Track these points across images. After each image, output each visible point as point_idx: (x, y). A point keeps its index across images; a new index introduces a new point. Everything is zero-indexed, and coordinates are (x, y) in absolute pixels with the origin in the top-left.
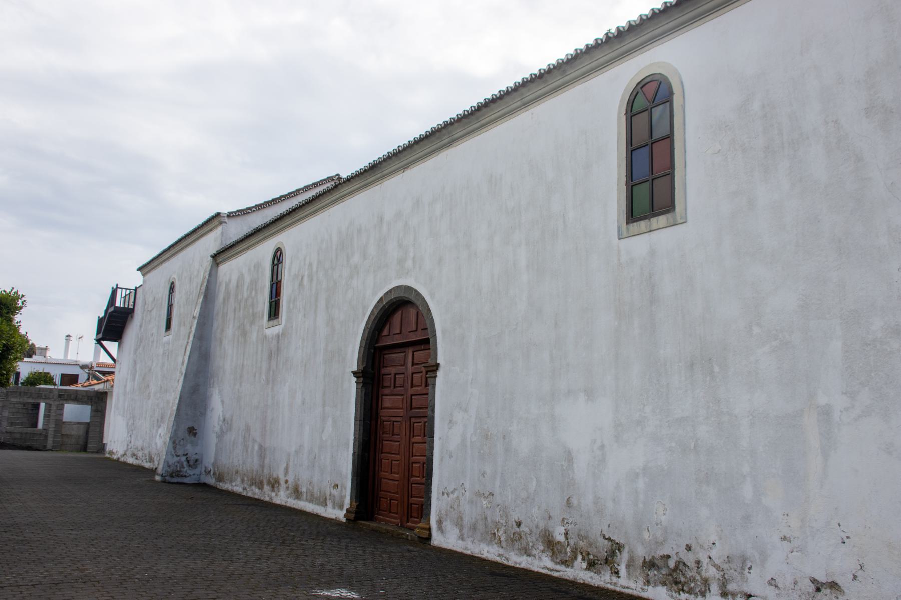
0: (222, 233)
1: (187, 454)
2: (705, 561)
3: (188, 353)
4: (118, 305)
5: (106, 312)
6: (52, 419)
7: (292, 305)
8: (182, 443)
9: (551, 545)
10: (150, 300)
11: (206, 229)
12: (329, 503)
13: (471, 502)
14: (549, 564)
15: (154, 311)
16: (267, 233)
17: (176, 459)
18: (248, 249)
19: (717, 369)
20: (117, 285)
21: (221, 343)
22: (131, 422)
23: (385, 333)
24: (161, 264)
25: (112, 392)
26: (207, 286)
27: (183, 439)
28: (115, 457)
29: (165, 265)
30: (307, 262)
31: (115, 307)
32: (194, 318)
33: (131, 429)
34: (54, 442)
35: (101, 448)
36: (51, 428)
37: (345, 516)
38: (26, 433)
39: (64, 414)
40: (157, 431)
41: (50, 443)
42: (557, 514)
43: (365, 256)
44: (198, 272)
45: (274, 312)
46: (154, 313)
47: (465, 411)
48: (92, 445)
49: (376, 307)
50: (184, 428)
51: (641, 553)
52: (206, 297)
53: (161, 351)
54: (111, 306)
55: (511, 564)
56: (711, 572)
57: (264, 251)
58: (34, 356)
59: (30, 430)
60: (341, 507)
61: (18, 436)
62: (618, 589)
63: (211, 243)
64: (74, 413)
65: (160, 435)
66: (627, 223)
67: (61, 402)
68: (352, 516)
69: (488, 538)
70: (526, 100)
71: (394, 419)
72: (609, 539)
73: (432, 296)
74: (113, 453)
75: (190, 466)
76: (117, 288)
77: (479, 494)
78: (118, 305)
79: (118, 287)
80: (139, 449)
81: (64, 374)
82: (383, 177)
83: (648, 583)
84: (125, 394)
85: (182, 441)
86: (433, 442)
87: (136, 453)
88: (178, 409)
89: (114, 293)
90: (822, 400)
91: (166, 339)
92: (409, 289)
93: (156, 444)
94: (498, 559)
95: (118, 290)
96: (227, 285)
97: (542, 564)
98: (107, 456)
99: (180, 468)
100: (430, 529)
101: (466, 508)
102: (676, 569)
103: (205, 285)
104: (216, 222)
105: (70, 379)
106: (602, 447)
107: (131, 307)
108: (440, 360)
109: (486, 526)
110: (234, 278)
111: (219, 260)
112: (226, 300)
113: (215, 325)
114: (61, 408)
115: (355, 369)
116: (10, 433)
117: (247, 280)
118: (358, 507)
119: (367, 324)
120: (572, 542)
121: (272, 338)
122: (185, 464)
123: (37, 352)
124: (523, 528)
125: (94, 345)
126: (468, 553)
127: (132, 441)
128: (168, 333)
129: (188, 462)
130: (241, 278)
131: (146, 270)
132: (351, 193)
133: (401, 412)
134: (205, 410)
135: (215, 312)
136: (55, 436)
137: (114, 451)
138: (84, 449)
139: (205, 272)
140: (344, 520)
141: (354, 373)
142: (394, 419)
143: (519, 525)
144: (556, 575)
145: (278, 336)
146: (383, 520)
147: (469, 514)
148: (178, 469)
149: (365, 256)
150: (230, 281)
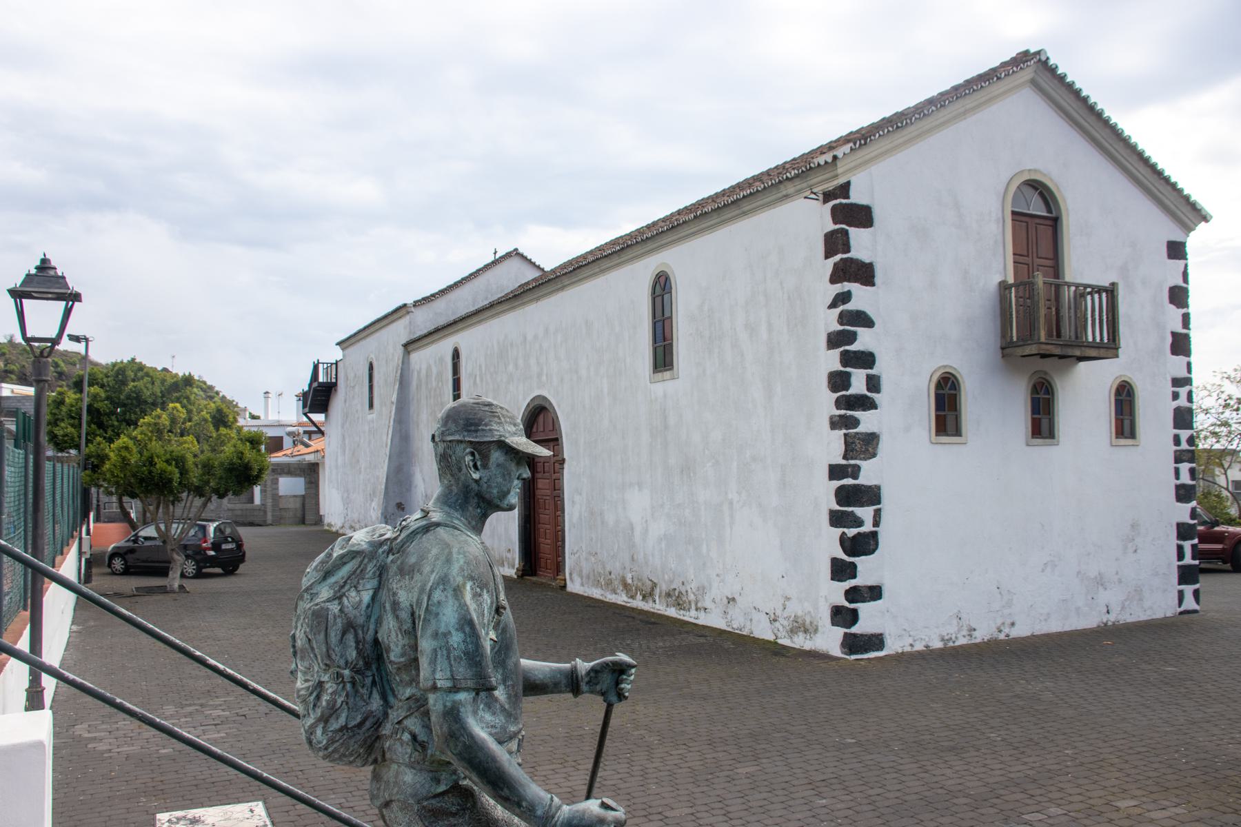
0: (410, 322)
2: (689, 590)
3: (390, 436)
4: (321, 379)
5: (310, 385)
6: (269, 494)
8: (392, 517)
9: (626, 586)
10: (351, 376)
11: (395, 316)
12: (505, 564)
13: (587, 559)
14: (625, 598)
15: (357, 387)
16: (446, 332)
18: (433, 342)
19: (692, 475)
21: (418, 426)
22: (346, 495)
23: (534, 430)
24: (358, 341)
25: (324, 463)
26: (401, 374)
28: (334, 529)
29: (363, 343)
31: (319, 383)
32: (392, 403)
33: (347, 502)
34: (273, 515)
35: (319, 520)
36: (269, 502)
37: (516, 574)
38: (247, 510)
39: (280, 488)
40: (370, 505)
41: (269, 518)
42: (628, 565)
43: (516, 366)
44: (393, 355)
46: (357, 389)
47: (580, 494)
48: (310, 517)
49: (525, 410)
50: (393, 504)
51: (664, 588)
52: (401, 383)
53: (367, 428)
54: (315, 381)
55: (607, 600)
56: (692, 597)
57: (444, 347)
59: (249, 506)
60: (513, 567)
61: (239, 513)
62: (656, 611)
63: (399, 332)
64: (289, 486)
67: (276, 476)
68: (520, 573)
69: (596, 583)
70: (602, 268)
71: (545, 498)
72: (651, 580)
73: (559, 406)
74: (332, 525)
76: (319, 363)
77: (590, 554)
78: (321, 379)
80: (356, 521)
82: (524, 304)
83: (667, 606)
84: (337, 467)
86: (564, 516)
87: (353, 525)
88: (386, 488)
89: (316, 368)
90: (730, 496)
91: (370, 417)
92: (544, 398)
93: (371, 517)
94: (601, 598)
96: (419, 373)
97: (621, 599)
98: (326, 528)
100: (565, 580)
101: (584, 564)
102: (678, 597)
103: (399, 372)
104: (403, 311)
107: (334, 380)
108: (566, 456)
109: (594, 575)
110: (424, 367)
111: (410, 348)
112: (419, 387)
113: (412, 409)
114: (276, 482)
116: (232, 510)
117: (434, 371)
118: (524, 566)
120: (635, 583)
124: (613, 576)
126: (586, 595)
127: (349, 513)
128: (371, 411)
130: (429, 368)
131: (345, 345)
132: (504, 312)
133: (548, 492)
134: (410, 486)
135: (411, 398)
136: (273, 511)
137: (333, 523)
138: (303, 521)
139: (398, 359)
140: (516, 577)
142: (545, 498)
143: (610, 573)
144: (628, 605)
146: (542, 575)
147: (586, 567)
149: (516, 366)
150: (420, 369)
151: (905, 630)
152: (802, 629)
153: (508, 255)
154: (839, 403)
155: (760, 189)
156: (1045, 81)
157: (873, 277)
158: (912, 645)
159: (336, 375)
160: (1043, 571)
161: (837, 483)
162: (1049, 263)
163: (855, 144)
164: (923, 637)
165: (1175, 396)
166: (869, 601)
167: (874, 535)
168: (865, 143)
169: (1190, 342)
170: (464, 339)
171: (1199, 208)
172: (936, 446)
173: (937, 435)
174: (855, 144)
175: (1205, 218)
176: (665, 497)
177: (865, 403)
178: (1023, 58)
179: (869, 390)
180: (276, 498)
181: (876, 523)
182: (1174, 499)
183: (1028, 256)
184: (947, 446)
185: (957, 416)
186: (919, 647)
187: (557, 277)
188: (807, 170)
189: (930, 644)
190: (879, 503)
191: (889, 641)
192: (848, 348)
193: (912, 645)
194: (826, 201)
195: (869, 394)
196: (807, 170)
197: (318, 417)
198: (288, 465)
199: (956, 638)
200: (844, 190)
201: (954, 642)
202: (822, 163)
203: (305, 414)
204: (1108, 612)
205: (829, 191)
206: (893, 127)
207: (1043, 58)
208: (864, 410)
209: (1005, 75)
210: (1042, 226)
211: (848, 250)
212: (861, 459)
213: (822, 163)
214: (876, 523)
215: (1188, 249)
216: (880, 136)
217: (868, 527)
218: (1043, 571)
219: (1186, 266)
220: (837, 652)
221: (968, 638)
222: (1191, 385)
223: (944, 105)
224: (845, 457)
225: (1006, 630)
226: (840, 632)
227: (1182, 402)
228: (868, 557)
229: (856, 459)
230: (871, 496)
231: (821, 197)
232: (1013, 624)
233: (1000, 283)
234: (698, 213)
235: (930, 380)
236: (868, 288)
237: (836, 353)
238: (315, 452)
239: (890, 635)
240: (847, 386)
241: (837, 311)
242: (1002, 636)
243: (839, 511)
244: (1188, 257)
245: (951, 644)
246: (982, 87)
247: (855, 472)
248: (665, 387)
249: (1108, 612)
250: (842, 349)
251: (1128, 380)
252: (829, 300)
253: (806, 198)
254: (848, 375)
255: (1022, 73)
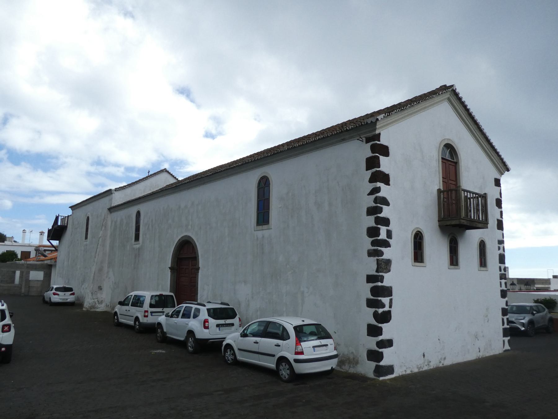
1: (98, 298)
5: (53, 227)
7: (144, 236)
17: (93, 300)
19: (278, 278)
20: (59, 215)
27: (96, 292)
30: (151, 219)
40: (81, 286)
45: (137, 238)
47: (208, 285)
57: (133, 211)
58: (5, 242)
65: (83, 288)
66: (257, 225)
75: (99, 303)
76: (59, 216)
78: (59, 224)
79: (59, 215)
81: (23, 251)
85: (95, 292)
89: (57, 218)
91: (85, 243)
92: (189, 237)
95: (59, 217)
99: (95, 304)
105: (25, 255)
106: (248, 301)
107: (66, 225)
115: (170, 266)
119: (174, 248)
121: (136, 249)
122: (97, 302)
123: (7, 239)
125: (39, 235)
129: (98, 302)
141: (170, 268)
145: (139, 248)
148: (94, 305)
151: (403, 363)
152: (348, 361)
153: (162, 171)
154: (373, 243)
155: (329, 135)
156: (453, 99)
157: (389, 181)
158: (405, 371)
159: (67, 222)
160: (455, 331)
161: (372, 285)
162: (453, 183)
163: (385, 115)
164: (410, 366)
165: (499, 248)
166: (388, 348)
167: (389, 312)
168: (389, 115)
169: (503, 224)
170: (143, 208)
171: (506, 164)
172: (414, 267)
173: (415, 262)
174: (385, 115)
175: (508, 170)
176: (261, 289)
177: (386, 244)
178: (444, 88)
179: (387, 237)
180: (28, 281)
181: (390, 307)
182: (500, 297)
183: (446, 179)
184: (419, 267)
185: (421, 252)
186: (408, 372)
187: (202, 178)
188: (360, 126)
189: (413, 370)
190: (392, 296)
191: (396, 369)
192: (379, 215)
193: (405, 371)
194: (367, 141)
195: (387, 239)
196: (360, 126)
197: (55, 243)
198: (36, 265)
199: (423, 366)
200: (378, 137)
201: (422, 368)
202: (369, 122)
203: (48, 240)
204: (479, 352)
205: (370, 137)
206: (400, 109)
207: (454, 89)
208: (385, 248)
209: (441, 94)
210: (451, 166)
211: (379, 167)
212: (384, 273)
213: (369, 122)
214: (390, 307)
215: (501, 182)
216: (395, 112)
217: (387, 308)
218: (455, 331)
219: (501, 190)
220: (371, 375)
221: (428, 366)
222: (504, 244)
223: (419, 103)
224: (377, 271)
225: (442, 362)
226: (373, 364)
227: (501, 251)
228: (387, 324)
229: (382, 272)
230: (388, 291)
231: (364, 141)
232: (445, 358)
233: (438, 190)
234: (290, 147)
235: (412, 234)
236: (387, 186)
237: (372, 218)
238: (51, 259)
239: (396, 366)
240: (378, 235)
241: (373, 197)
242: (441, 365)
243: (373, 299)
244: (501, 186)
245: (421, 370)
246: (433, 97)
247: (381, 279)
248: (263, 233)
249: (479, 352)
250: (376, 216)
251: (483, 240)
252: (368, 191)
253: (358, 139)
254: (379, 229)
255: (444, 95)
